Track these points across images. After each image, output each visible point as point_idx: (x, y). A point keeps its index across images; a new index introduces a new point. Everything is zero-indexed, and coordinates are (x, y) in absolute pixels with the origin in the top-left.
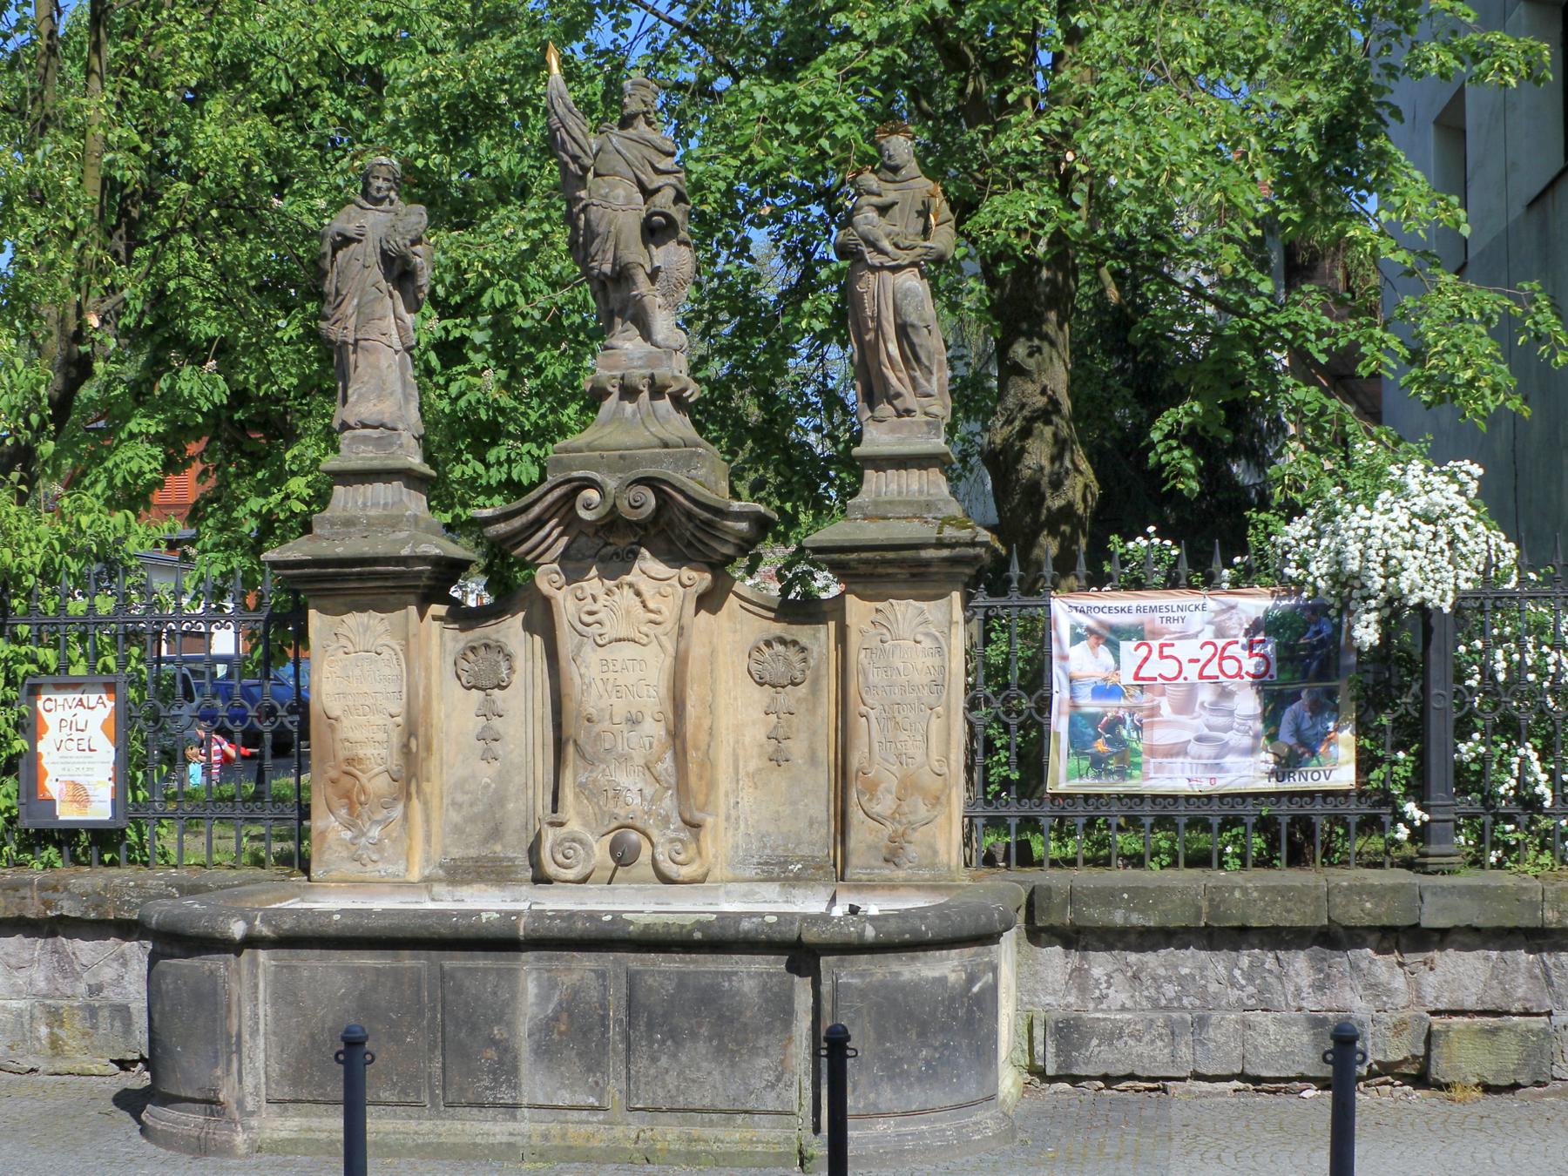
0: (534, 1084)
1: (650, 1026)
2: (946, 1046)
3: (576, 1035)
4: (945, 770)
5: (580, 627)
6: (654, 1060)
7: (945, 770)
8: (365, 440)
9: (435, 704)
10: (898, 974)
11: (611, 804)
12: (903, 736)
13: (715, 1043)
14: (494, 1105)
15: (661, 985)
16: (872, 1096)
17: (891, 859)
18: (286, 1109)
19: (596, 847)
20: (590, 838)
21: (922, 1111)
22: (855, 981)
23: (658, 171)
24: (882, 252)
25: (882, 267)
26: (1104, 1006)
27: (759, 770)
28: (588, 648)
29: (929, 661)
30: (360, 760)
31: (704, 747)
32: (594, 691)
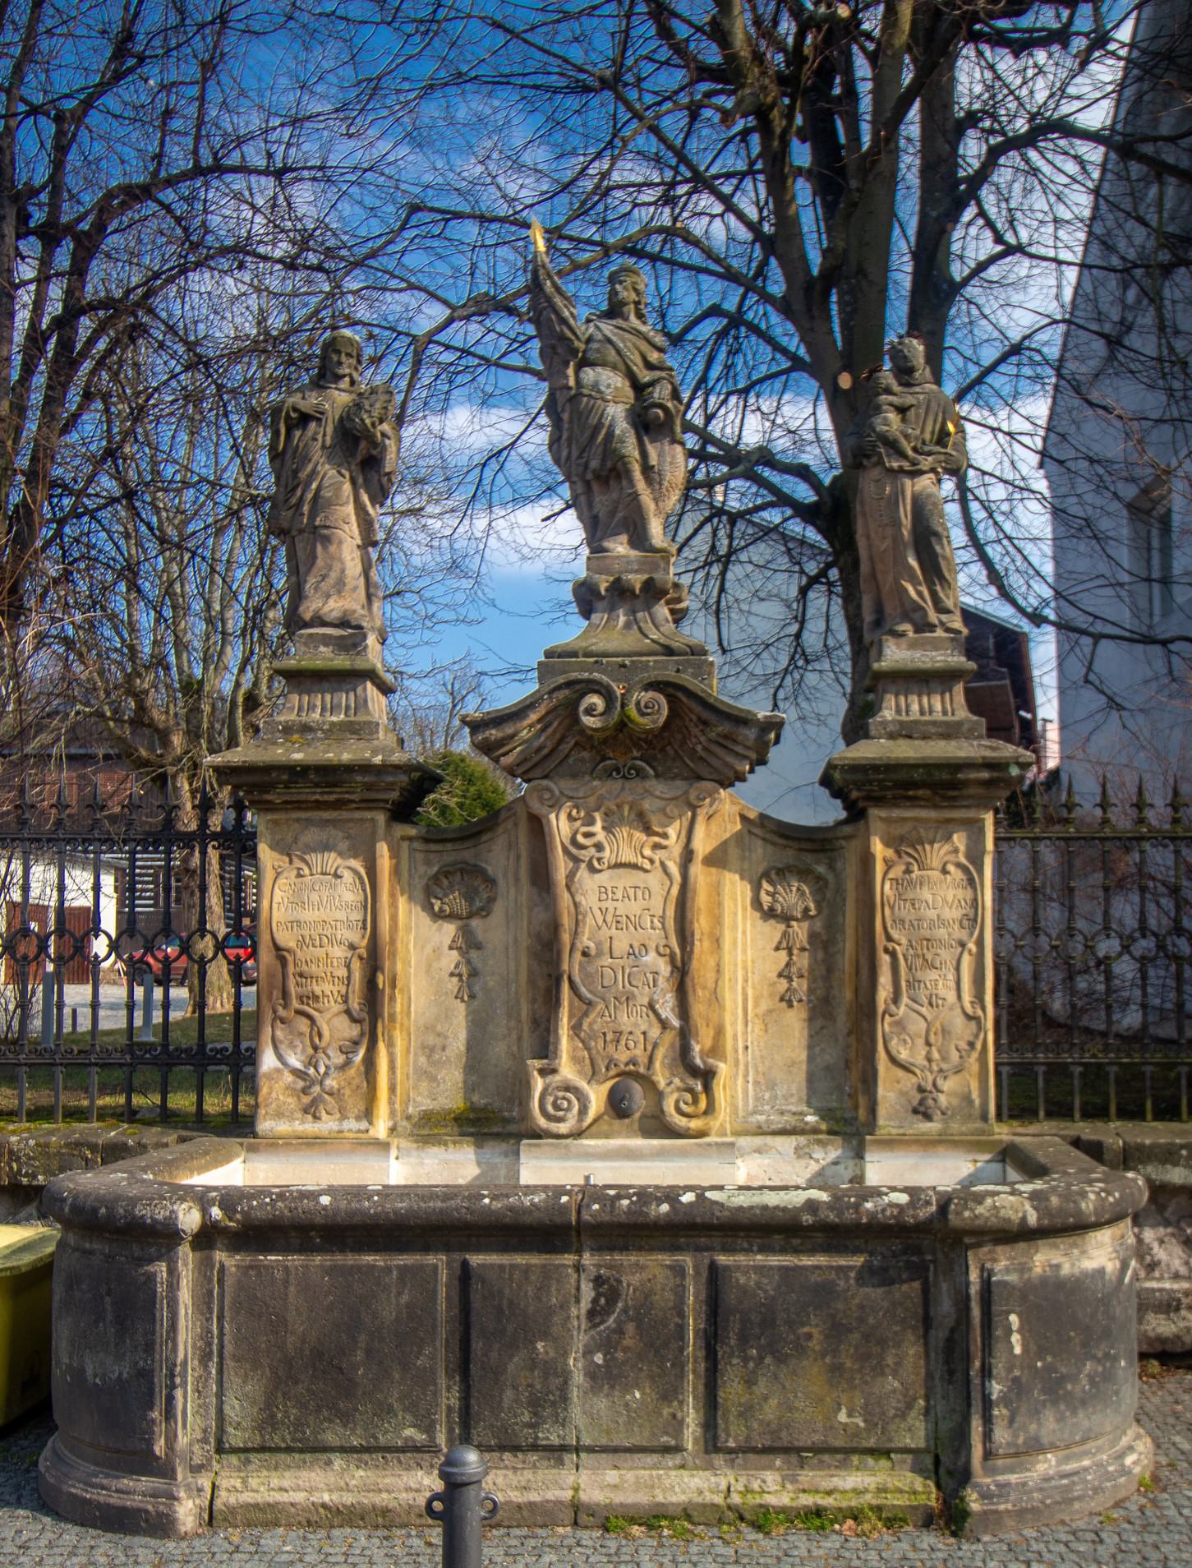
0: (586, 1412)
1: (744, 1339)
2: (1107, 1355)
3: (640, 1346)
4: (980, 1013)
5: (574, 851)
6: (750, 1382)
7: (980, 1013)
8: (326, 640)
9: (401, 933)
10: (1058, 1266)
11: (611, 1048)
12: (933, 975)
13: (828, 1360)
14: (535, 1448)
15: (758, 1284)
16: (1033, 1427)
17: (922, 1111)
18: (248, 1462)
19: (593, 1097)
20: (583, 1084)
21: (1084, 1441)
22: (1012, 1278)
23: (650, 366)
24: (904, 456)
25: (901, 470)
26: (1157, 1274)
27: (770, 1011)
28: (583, 872)
29: (960, 893)
30: (316, 998)
31: (711, 984)
32: (589, 920)
